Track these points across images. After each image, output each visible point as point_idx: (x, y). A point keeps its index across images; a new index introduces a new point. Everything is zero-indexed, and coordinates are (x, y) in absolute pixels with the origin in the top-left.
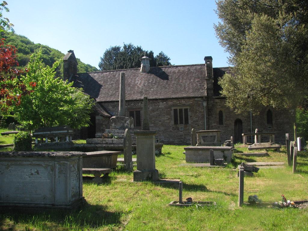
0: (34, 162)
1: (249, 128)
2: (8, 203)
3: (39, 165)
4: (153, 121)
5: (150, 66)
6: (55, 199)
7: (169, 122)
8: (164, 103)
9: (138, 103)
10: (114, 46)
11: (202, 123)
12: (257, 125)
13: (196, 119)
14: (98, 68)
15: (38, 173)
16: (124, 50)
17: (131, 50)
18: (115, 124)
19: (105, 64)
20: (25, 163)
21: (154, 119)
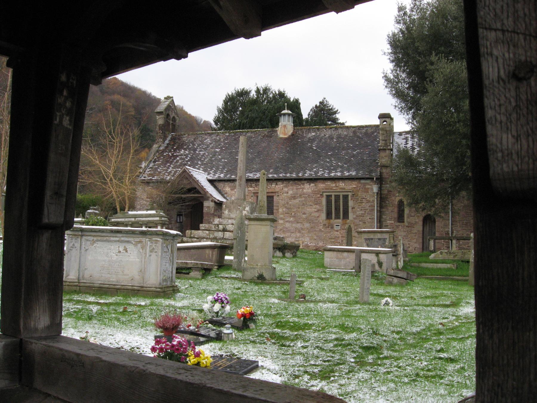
0: (122, 239)
1: (446, 230)
2: (92, 283)
3: (128, 242)
4: (293, 214)
5: (294, 126)
6: (143, 279)
7: (318, 215)
8: (312, 185)
9: (272, 185)
10: (239, 87)
11: (370, 219)
12: (460, 226)
13: (361, 212)
14: (214, 125)
15: (126, 251)
16: (256, 96)
17: (268, 97)
18: (229, 211)
19: (224, 118)
20: (112, 239)
21: (295, 210)
